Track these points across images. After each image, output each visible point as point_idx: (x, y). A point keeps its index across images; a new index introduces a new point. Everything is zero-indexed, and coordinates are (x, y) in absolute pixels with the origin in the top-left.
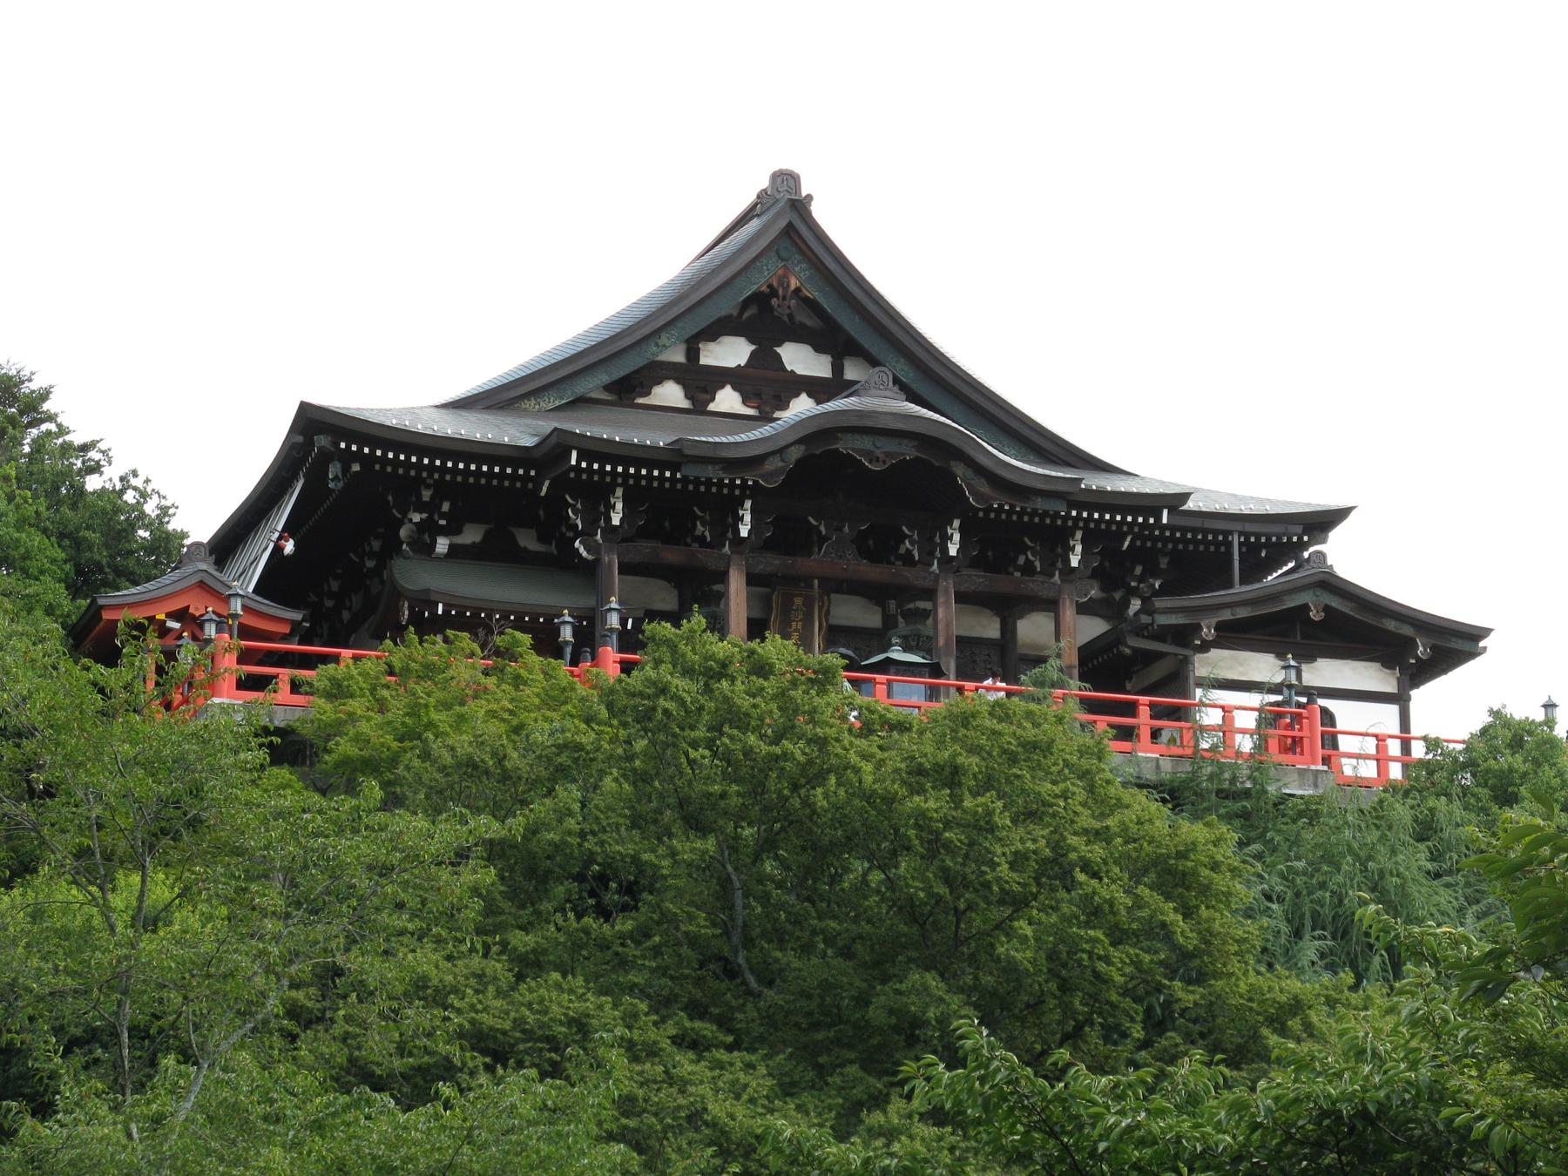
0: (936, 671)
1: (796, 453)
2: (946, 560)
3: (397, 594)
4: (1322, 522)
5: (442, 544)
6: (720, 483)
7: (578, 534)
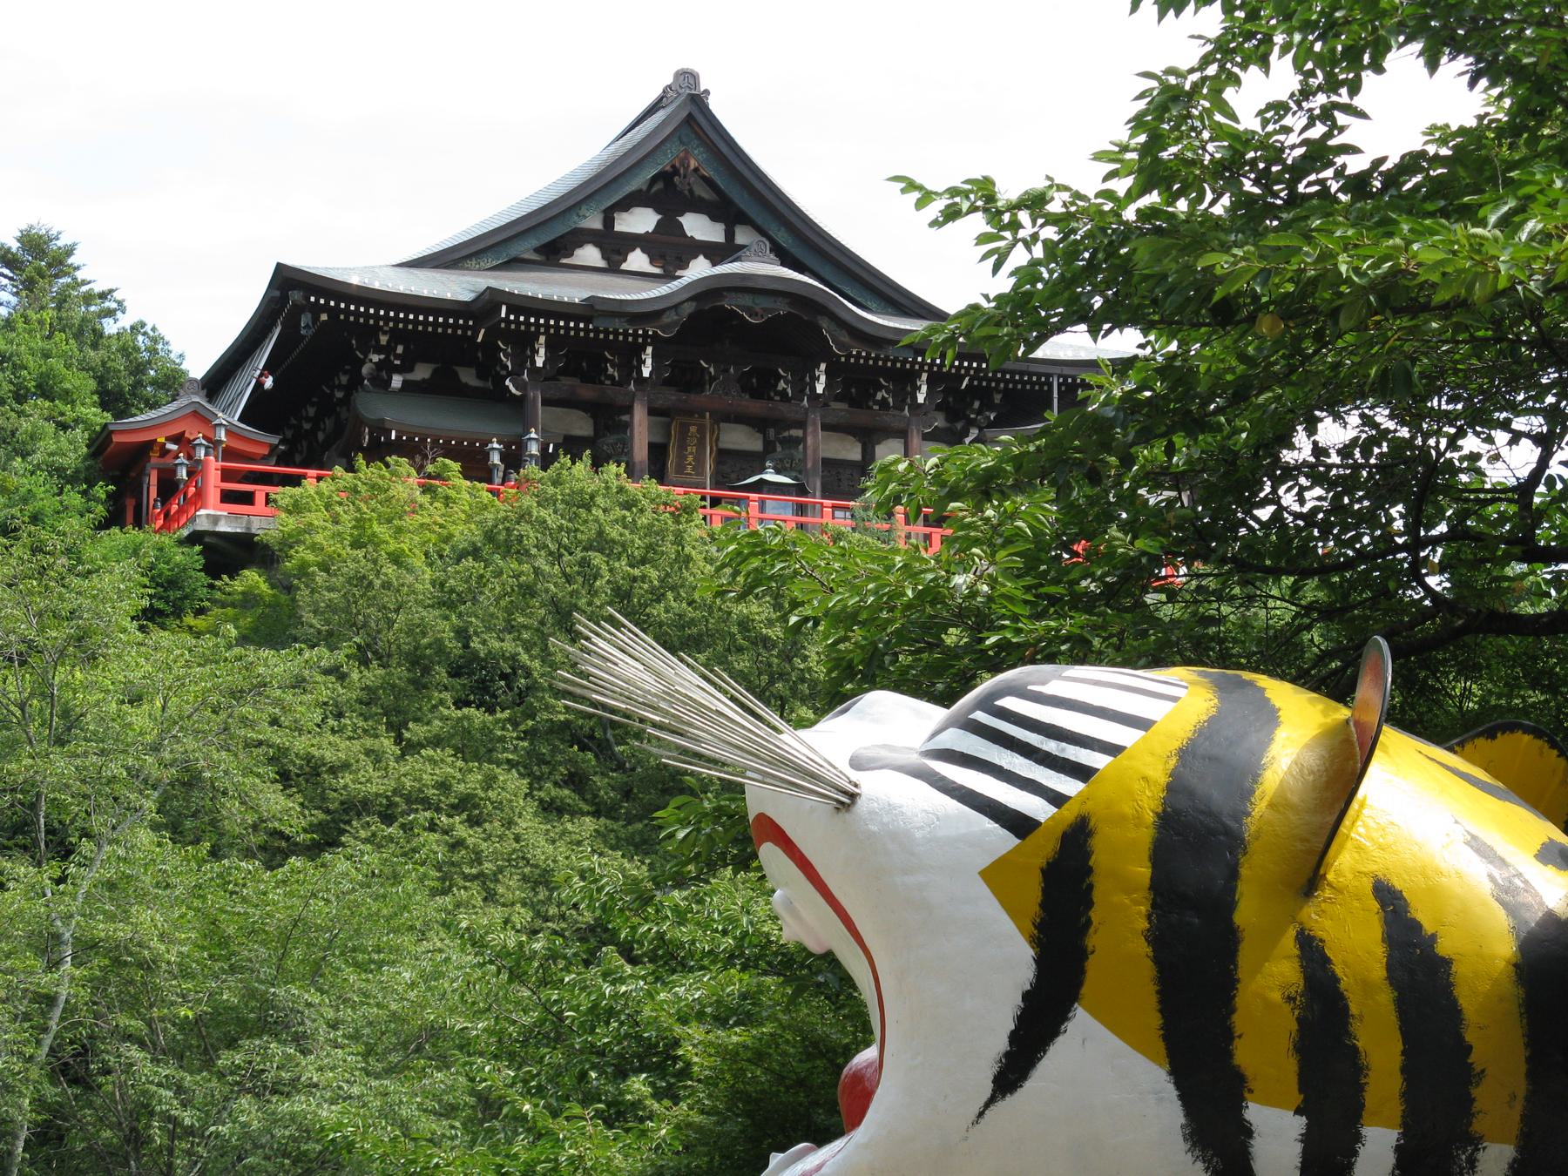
0: (801, 490)
1: (689, 308)
2: (814, 396)
3: (360, 422)
5: (397, 381)
6: (905, 361)
7: (509, 374)
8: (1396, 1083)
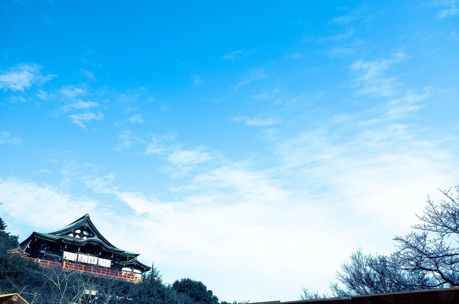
4: (137, 255)
5: (45, 248)
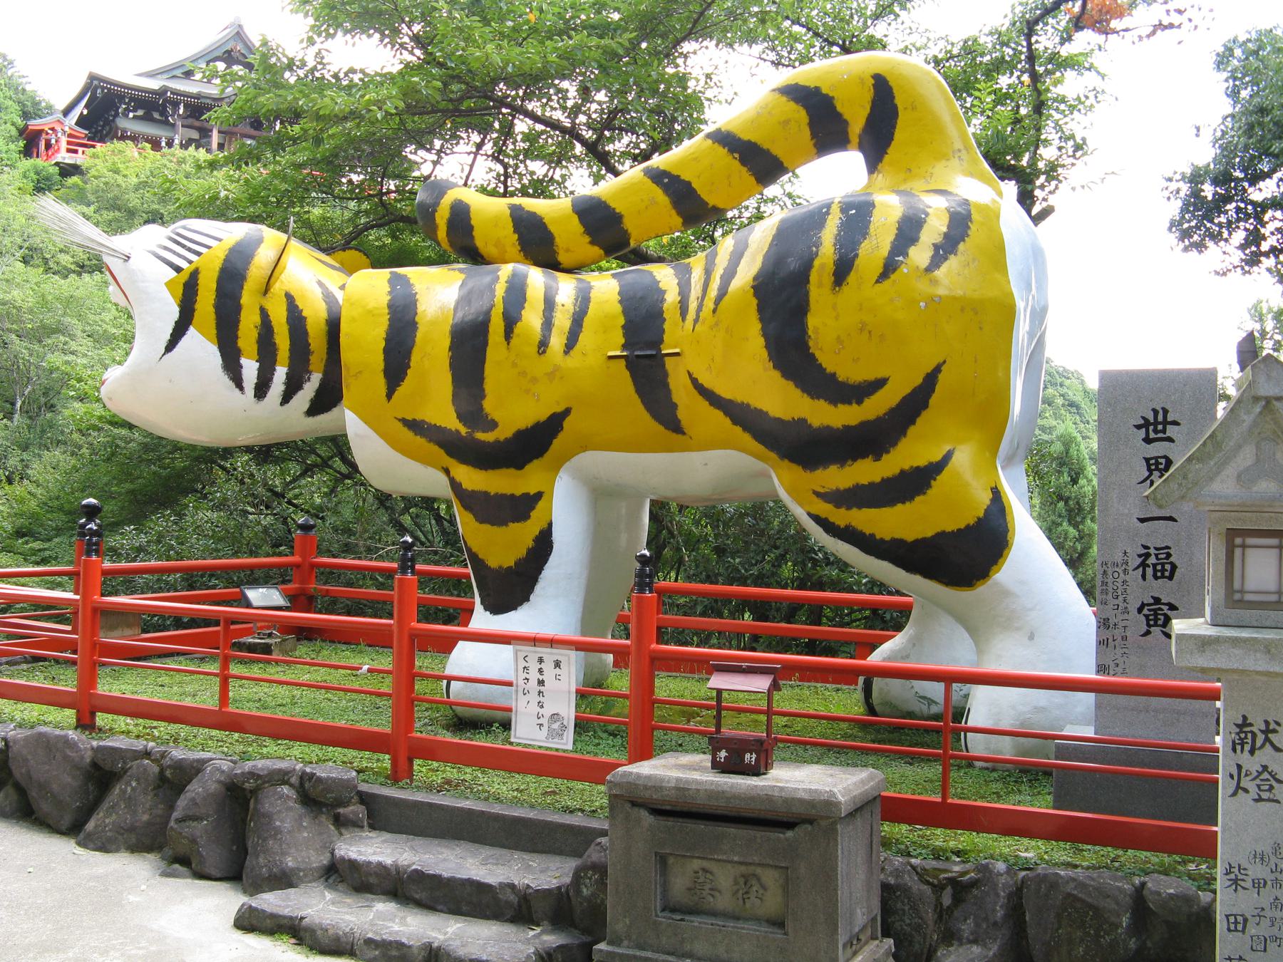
3: (117, 128)
5: (131, 115)
8: (287, 354)
